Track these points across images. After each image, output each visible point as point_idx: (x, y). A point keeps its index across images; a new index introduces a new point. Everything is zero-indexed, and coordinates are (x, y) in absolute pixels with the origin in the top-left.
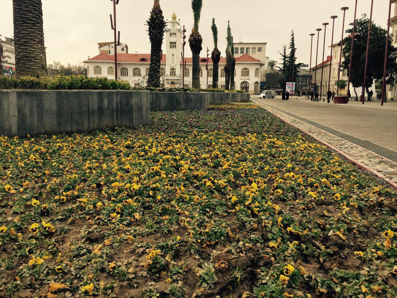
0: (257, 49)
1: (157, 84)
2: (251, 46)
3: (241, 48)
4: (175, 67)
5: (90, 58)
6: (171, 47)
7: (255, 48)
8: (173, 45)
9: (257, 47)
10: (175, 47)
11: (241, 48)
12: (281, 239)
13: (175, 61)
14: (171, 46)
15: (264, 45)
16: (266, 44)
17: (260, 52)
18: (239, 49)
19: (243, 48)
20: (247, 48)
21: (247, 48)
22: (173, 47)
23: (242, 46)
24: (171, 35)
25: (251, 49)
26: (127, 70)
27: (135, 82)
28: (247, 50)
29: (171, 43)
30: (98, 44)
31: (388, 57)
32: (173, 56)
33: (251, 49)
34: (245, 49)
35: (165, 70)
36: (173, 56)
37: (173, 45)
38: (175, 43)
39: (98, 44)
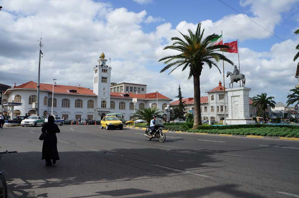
0: (141, 89)
1: (193, 104)
2: (137, 87)
3: (131, 87)
4: (106, 100)
5: (17, 85)
6: (102, 82)
7: (140, 88)
8: (104, 80)
9: (141, 87)
10: (106, 82)
11: (131, 87)
12: (277, 109)
13: (106, 94)
14: (102, 80)
15: (145, 86)
16: (146, 85)
17: (143, 92)
18: (133, 88)
19: (128, 87)
20: (134, 88)
21: (134, 88)
22: (104, 82)
23: (135, 86)
24: (102, 71)
25: (137, 88)
26: (82, 101)
27: (64, 113)
28: (134, 89)
29: (103, 78)
30: (237, 82)
31: (123, 97)
32: (104, 89)
33: (137, 88)
34: (133, 88)
35: (69, 101)
36: (104, 89)
37: (104, 80)
38: (106, 78)
39: (237, 82)
